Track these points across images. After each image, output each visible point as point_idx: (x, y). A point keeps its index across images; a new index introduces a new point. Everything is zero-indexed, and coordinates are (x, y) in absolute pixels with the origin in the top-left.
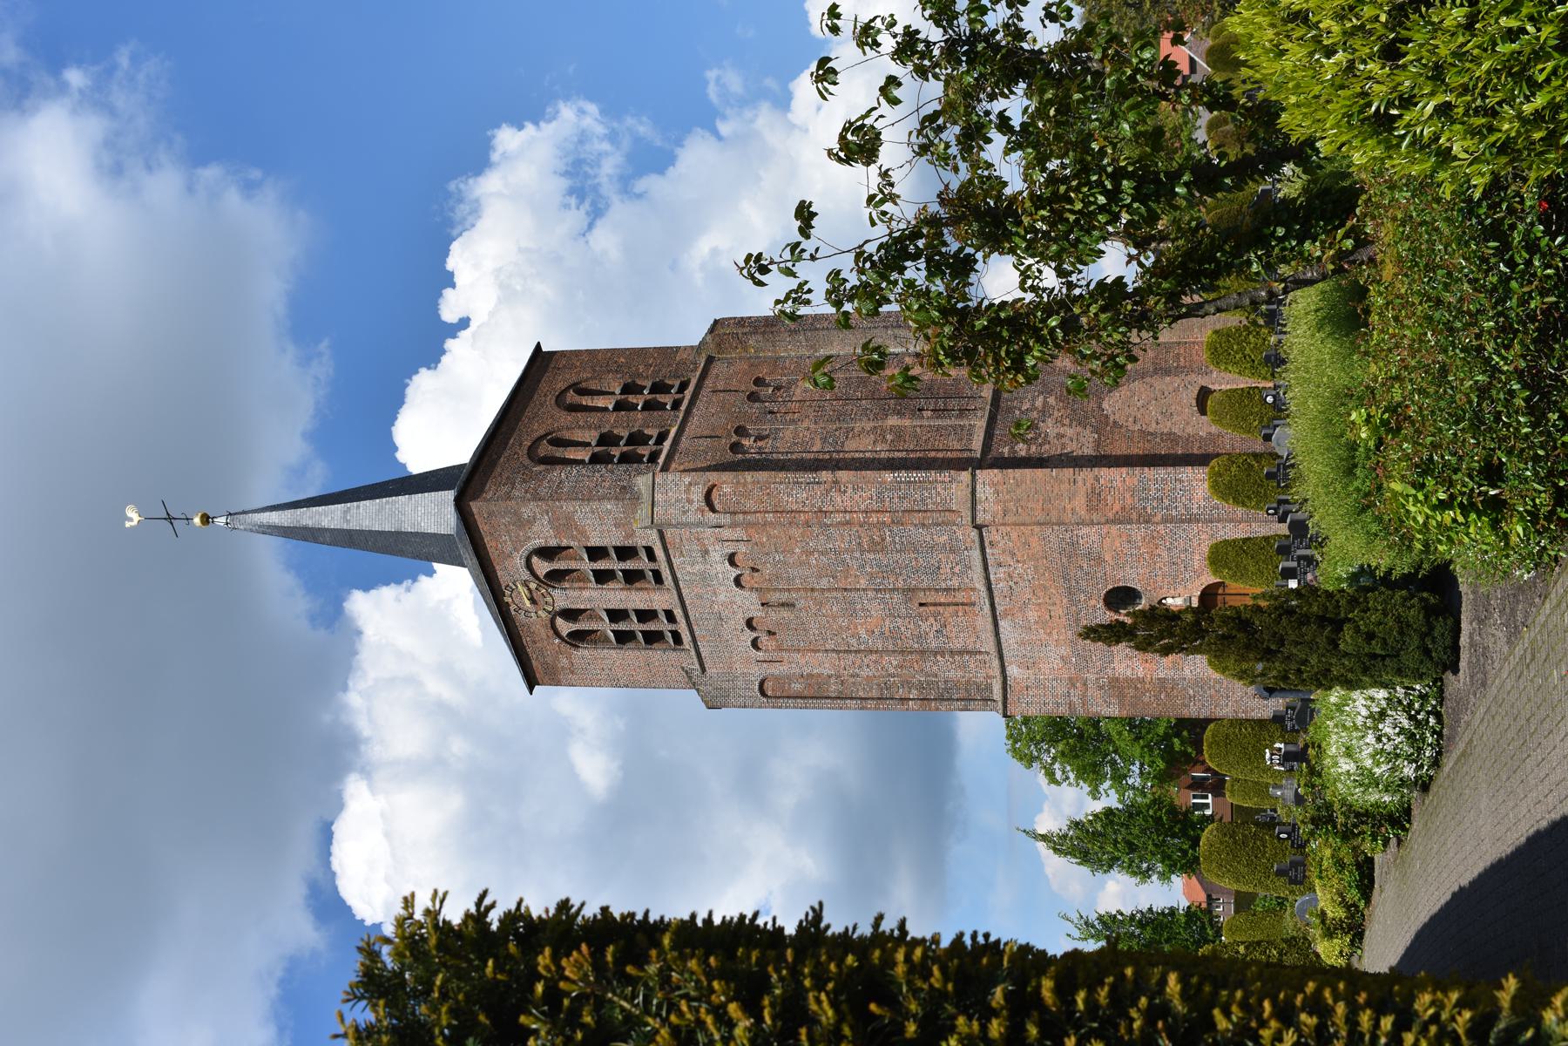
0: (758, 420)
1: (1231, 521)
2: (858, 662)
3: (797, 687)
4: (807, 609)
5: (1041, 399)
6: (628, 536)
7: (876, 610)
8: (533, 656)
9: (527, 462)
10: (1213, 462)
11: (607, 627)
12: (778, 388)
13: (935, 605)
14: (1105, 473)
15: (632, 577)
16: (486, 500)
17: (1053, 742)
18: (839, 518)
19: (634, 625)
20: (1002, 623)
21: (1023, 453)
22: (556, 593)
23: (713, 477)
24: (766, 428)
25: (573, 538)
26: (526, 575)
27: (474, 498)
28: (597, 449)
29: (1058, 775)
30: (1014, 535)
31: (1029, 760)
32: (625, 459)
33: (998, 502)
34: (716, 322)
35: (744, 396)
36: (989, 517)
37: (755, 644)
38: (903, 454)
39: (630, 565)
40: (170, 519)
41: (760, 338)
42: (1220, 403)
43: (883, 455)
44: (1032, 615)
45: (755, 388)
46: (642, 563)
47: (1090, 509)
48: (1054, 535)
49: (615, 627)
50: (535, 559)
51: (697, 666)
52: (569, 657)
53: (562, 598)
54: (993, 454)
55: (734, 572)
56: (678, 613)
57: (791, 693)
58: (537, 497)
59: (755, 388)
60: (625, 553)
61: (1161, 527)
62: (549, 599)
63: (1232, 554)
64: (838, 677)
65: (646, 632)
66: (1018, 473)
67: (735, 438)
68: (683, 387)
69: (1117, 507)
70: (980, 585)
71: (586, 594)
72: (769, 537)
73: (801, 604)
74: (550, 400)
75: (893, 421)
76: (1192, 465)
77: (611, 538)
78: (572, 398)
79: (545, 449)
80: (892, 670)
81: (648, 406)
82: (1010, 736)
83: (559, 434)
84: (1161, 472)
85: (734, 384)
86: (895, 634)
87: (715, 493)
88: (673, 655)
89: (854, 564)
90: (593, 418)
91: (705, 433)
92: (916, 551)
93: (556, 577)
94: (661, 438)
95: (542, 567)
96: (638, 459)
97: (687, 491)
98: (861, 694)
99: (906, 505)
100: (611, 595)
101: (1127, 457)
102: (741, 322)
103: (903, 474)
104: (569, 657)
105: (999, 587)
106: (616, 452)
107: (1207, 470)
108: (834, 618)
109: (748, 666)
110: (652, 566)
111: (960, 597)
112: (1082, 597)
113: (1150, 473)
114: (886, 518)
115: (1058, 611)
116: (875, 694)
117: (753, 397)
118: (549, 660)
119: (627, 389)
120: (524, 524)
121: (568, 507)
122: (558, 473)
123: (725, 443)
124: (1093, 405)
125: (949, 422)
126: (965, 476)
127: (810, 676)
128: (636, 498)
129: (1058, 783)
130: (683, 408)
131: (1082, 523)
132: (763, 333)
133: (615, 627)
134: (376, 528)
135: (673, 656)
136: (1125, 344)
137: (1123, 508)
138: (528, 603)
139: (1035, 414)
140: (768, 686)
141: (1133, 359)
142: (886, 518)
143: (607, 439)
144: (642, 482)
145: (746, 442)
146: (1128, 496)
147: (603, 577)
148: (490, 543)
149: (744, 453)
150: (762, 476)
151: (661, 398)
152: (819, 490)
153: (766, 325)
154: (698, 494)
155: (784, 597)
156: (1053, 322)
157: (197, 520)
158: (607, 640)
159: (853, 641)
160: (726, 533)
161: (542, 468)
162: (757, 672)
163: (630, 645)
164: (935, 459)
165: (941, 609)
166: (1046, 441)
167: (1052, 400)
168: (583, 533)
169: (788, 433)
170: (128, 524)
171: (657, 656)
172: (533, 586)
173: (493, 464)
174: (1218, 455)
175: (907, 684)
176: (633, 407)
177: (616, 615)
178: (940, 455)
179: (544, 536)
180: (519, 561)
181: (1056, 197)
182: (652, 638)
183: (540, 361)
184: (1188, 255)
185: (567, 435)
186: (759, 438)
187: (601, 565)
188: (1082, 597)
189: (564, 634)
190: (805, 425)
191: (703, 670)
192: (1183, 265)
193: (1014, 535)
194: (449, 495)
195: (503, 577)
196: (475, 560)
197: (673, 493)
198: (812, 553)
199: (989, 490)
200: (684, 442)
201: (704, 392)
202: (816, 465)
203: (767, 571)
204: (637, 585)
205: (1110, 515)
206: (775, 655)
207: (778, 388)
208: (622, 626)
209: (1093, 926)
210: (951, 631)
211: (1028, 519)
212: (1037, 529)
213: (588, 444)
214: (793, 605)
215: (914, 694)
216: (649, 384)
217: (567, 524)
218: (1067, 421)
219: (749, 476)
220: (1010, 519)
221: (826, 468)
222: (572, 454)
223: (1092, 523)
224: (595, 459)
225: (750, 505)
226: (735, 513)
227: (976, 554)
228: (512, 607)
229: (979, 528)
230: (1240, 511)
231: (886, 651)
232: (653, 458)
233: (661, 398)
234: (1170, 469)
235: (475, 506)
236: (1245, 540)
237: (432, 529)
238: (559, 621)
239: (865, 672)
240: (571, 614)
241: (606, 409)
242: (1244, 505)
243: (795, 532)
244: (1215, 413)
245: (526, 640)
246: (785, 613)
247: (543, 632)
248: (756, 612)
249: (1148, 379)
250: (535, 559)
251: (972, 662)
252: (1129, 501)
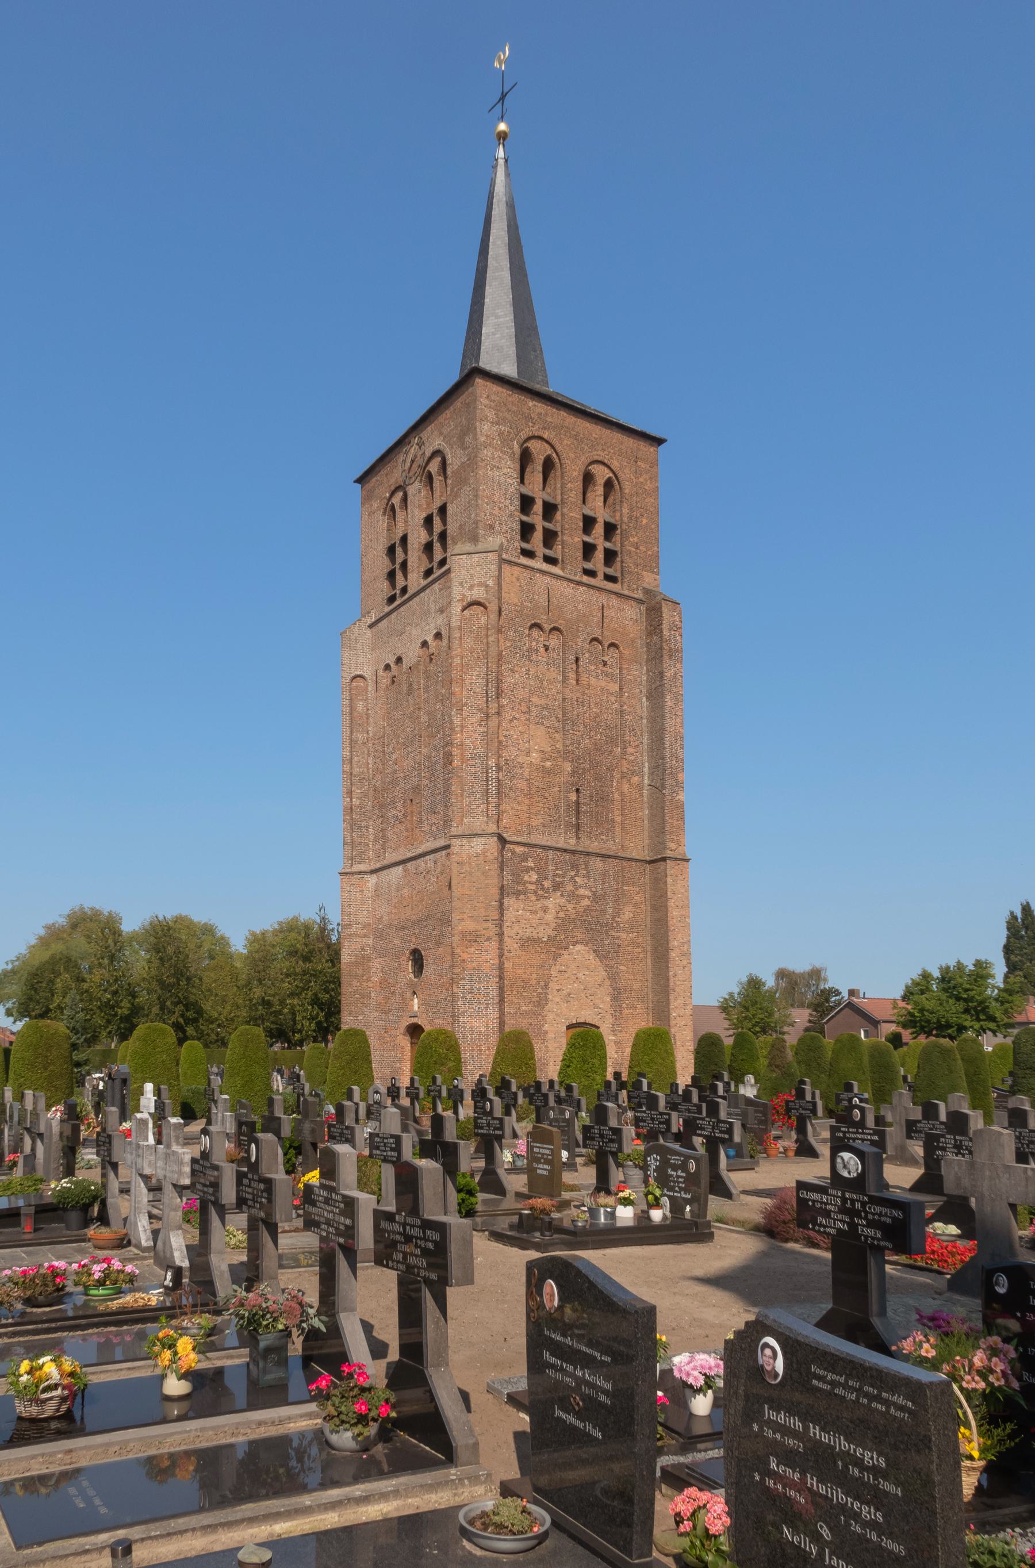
3: (360, 706)
5: (587, 893)
9: (523, 435)
20: (400, 868)
23: (493, 607)
35: (597, 634)
44: (405, 892)
52: (378, 508)
69: (465, 956)
91: (554, 600)
97: (480, 584)
112: (417, 931)
116: (356, 770)
124: (580, 936)
137: (464, 961)
139: (570, 887)
140: (360, 683)
146: (474, 964)
152: (482, 702)
154: (478, 594)
157: (502, 127)
167: (586, 902)
188: (417, 931)
199: (479, 849)
215: (356, 802)
218: (562, 915)
248: (406, 663)
249: (608, 983)
252: (469, 965)
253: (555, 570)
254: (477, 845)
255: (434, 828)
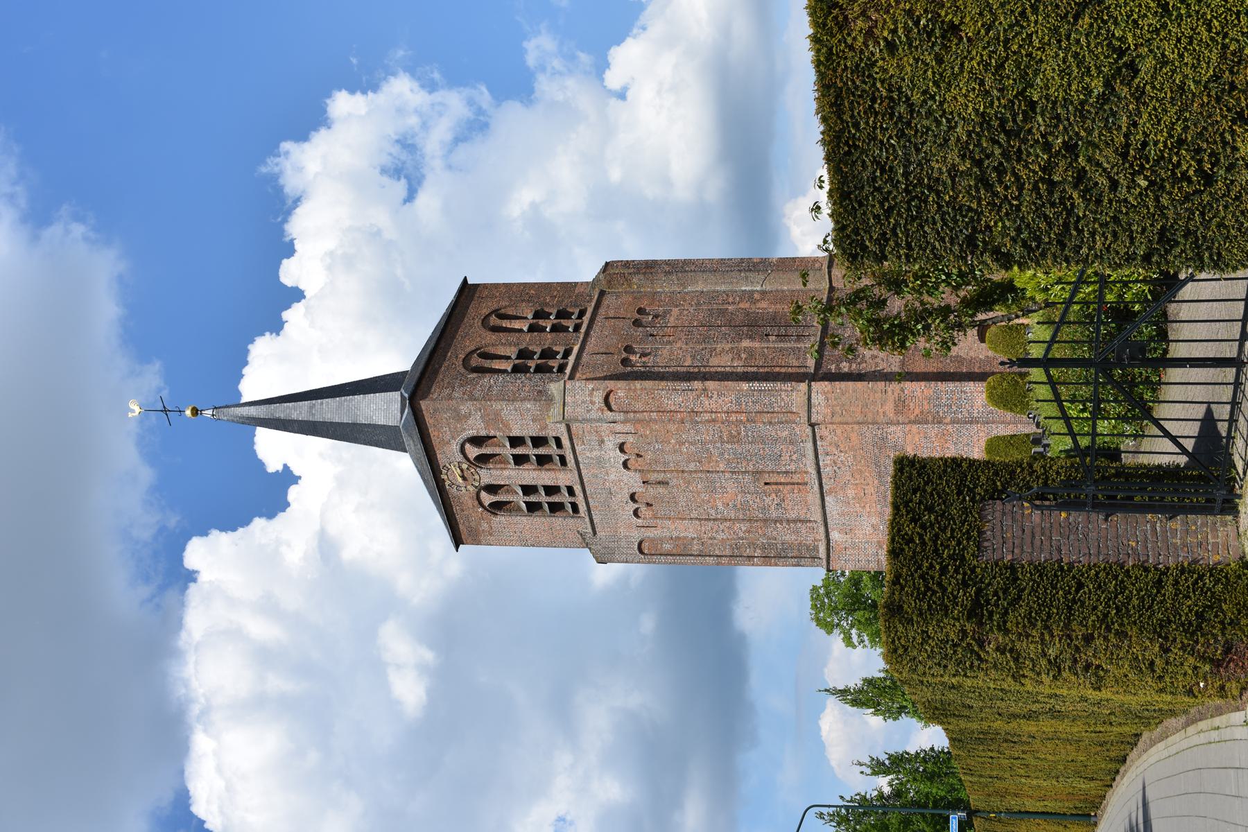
0: (641, 341)
1: (1003, 422)
2: (716, 528)
3: (667, 547)
4: (678, 486)
6: (542, 429)
7: (731, 487)
8: (461, 522)
9: (463, 370)
10: (990, 379)
11: (520, 499)
12: (656, 316)
13: (776, 484)
14: (908, 386)
15: (543, 460)
16: (432, 400)
17: (851, 612)
18: (707, 416)
19: (542, 498)
20: (827, 499)
21: (846, 370)
22: (483, 472)
23: (611, 384)
24: (648, 347)
25: (499, 429)
26: (460, 458)
27: (424, 397)
28: (517, 362)
29: (855, 639)
30: (839, 432)
31: (829, 627)
32: (539, 369)
33: (827, 406)
34: (607, 264)
35: (630, 322)
36: (820, 418)
37: (636, 513)
38: (755, 369)
39: (542, 451)
40: (165, 410)
41: (642, 277)
42: (996, 335)
43: (739, 370)
44: (851, 493)
45: (638, 316)
46: (552, 450)
47: (897, 413)
48: (869, 432)
49: (527, 499)
50: (468, 446)
51: (590, 530)
52: (489, 523)
53: (487, 476)
54: (823, 370)
55: (623, 457)
56: (577, 489)
57: (663, 551)
58: (472, 398)
59: (638, 316)
60: (539, 441)
61: (949, 427)
62: (477, 477)
63: (1002, 446)
64: (699, 539)
65: (550, 503)
66: (843, 384)
67: (624, 355)
68: (582, 314)
69: (917, 411)
70: (812, 470)
71: (506, 473)
72: (651, 430)
73: (673, 482)
74: (477, 322)
75: (746, 343)
76: (973, 380)
77: (527, 429)
78: (494, 320)
79: (476, 361)
80: (741, 534)
81: (555, 329)
82: (814, 607)
83: (486, 349)
84: (951, 386)
85: (622, 313)
86: (745, 507)
87: (612, 398)
88: (571, 521)
89: (715, 452)
90: (513, 337)
91: (602, 350)
92: (763, 442)
93: (483, 459)
94: (567, 353)
95: (473, 452)
96: (549, 370)
97: (591, 395)
98: (717, 552)
99: (758, 408)
100: (526, 474)
101: (925, 373)
102: (627, 264)
103: (756, 384)
104: (489, 523)
105: (826, 471)
106: (532, 364)
107: (985, 384)
108: (699, 493)
109: (629, 530)
110: (560, 452)
111: (796, 478)
113: (942, 386)
114: (743, 417)
115: (870, 490)
116: (728, 552)
117: (637, 323)
118: (473, 524)
119: (537, 315)
120: (460, 418)
121: (497, 406)
122: (487, 380)
123: (617, 358)
125: (789, 345)
126: (803, 386)
127: (678, 538)
128: (550, 400)
129: (854, 647)
130: (583, 330)
131: (892, 423)
132: (644, 274)
133: (527, 499)
134: (337, 420)
135: (571, 522)
136: (952, 338)
137: (922, 412)
138: (460, 480)
140: (645, 546)
141: (955, 344)
142: (743, 417)
143: (524, 354)
144: (555, 388)
145: (633, 358)
146: (925, 403)
147: (520, 460)
148: (433, 433)
149: (632, 366)
150: (648, 384)
151: (564, 322)
152: (691, 395)
153: (647, 267)
154: (598, 398)
155: (661, 477)
156: (919, 327)
157: (188, 412)
158: (519, 509)
159: (712, 512)
160: (619, 427)
161: (475, 375)
162: (636, 535)
163: (537, 513)
164: (779, 373)
165: (781, 487)
166: (863, 361)
168: (507, 425)
169: (665, 352)
170: (130, 415)
171: (558, 521)
172: (465, 466)
173: (436, 372)
174: (993, 374)
175: (752, 544)
176: (543, 329)
177: (528, 490)
178: (783, 370)
179: (476, 427)
180: (455, 447)
181: (924, 276)
182: (556, 508)
183: (467, 291)
184: (980, 295)
185: (492, 350)
186: (643, 355)
187: (519, 451)
189: (486, 504)
190: (679, 345)
191: (595, 533)
192: (978, 300)
193: (839, 432)
194: (395, 396)
195: (442, 459)
196: (420, 446)
197: (581, 396)
198: (684, 443)
200: (585, 358)
201: (599, 318)
202: (688, 377)
203: (649, 456)
204: (547, 466)
205: (912, 417)
206: (652, 523)
207: (656, 316)
208: (533, 499)
209: (884, 764)
210: (788, 504)
211: (850, 420)
212: (856, 427)
213: (508, 358)
214: (667, 483)
215: (758, 553)
216: (554, 311)
217: (496, 418)
219: (638, 384)
220: (837, 419)
221: (696, 379)
222: (497, 365)
223: (898, 423)
224: (516, 369)
225: (639, 406)
226: (627, 412)
227: (810, 445)
228: (447, 483)
229: (812, 425)
230: (1009, 415)
231: (737, 520)
232: (561, 369)
233: (564, 322)
234: (957, 383)
235: (424, 404)
236: (1012, 436)
237: (382, 422)
238: (483, 494)
239: (721, 536)
240: (492, 489)
241: (521, 331)
242: (1011, 410)
243: (672, 427)
244: (991, 342)
245: (456, 509)
246: (661, 490)
247: (469, 502)
248: (639, 488)
250: (468, 446)
251: (803, 528)
252: (926, 407)
253: (576, 349)
254: (817, 399)
255: (794, 458)
